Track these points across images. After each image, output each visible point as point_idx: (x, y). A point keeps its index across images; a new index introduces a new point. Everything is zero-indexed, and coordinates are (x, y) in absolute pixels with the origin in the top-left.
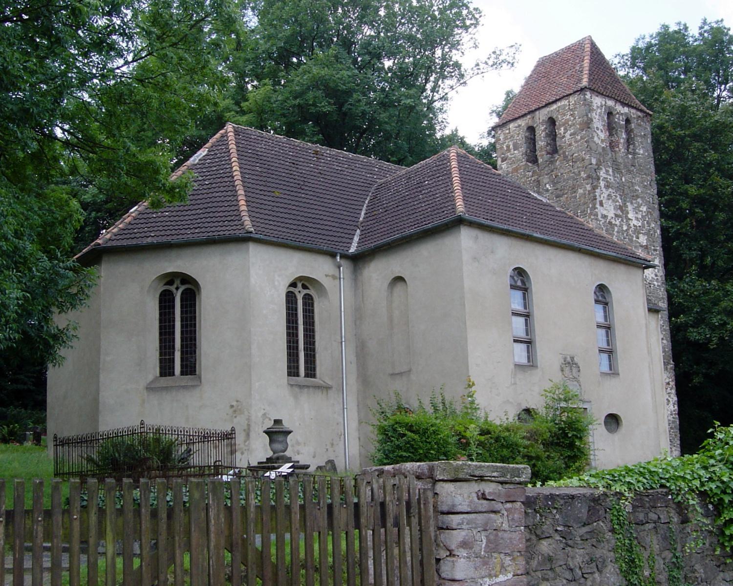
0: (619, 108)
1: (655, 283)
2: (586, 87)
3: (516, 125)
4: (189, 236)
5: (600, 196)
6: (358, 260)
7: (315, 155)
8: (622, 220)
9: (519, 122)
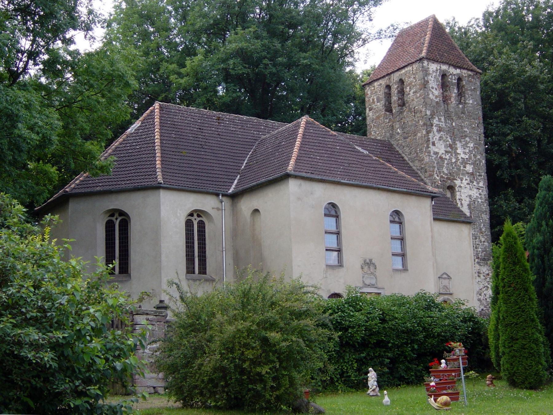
0: (452, 70)
1: (480, 200)
2: (423, 58)
3: (379, 83)
4: (122, 186)
5: (433, 138)
6: (234, 197)
7: (217, 121)
8: (452, 155)
9: (381, 81)
